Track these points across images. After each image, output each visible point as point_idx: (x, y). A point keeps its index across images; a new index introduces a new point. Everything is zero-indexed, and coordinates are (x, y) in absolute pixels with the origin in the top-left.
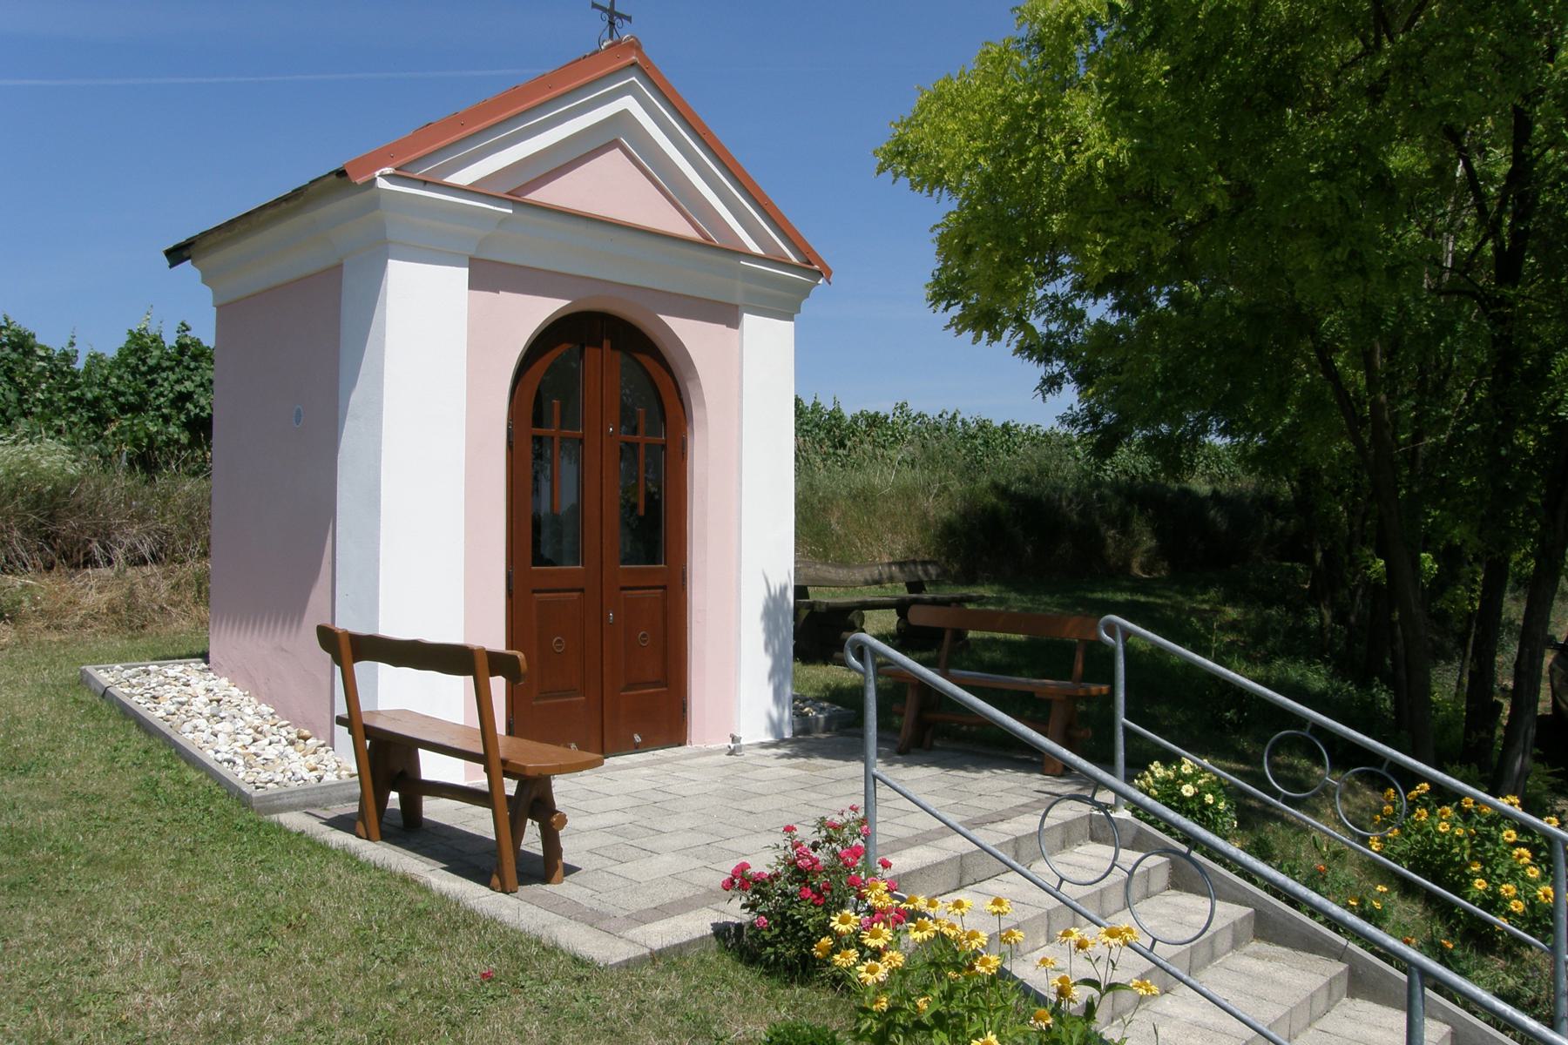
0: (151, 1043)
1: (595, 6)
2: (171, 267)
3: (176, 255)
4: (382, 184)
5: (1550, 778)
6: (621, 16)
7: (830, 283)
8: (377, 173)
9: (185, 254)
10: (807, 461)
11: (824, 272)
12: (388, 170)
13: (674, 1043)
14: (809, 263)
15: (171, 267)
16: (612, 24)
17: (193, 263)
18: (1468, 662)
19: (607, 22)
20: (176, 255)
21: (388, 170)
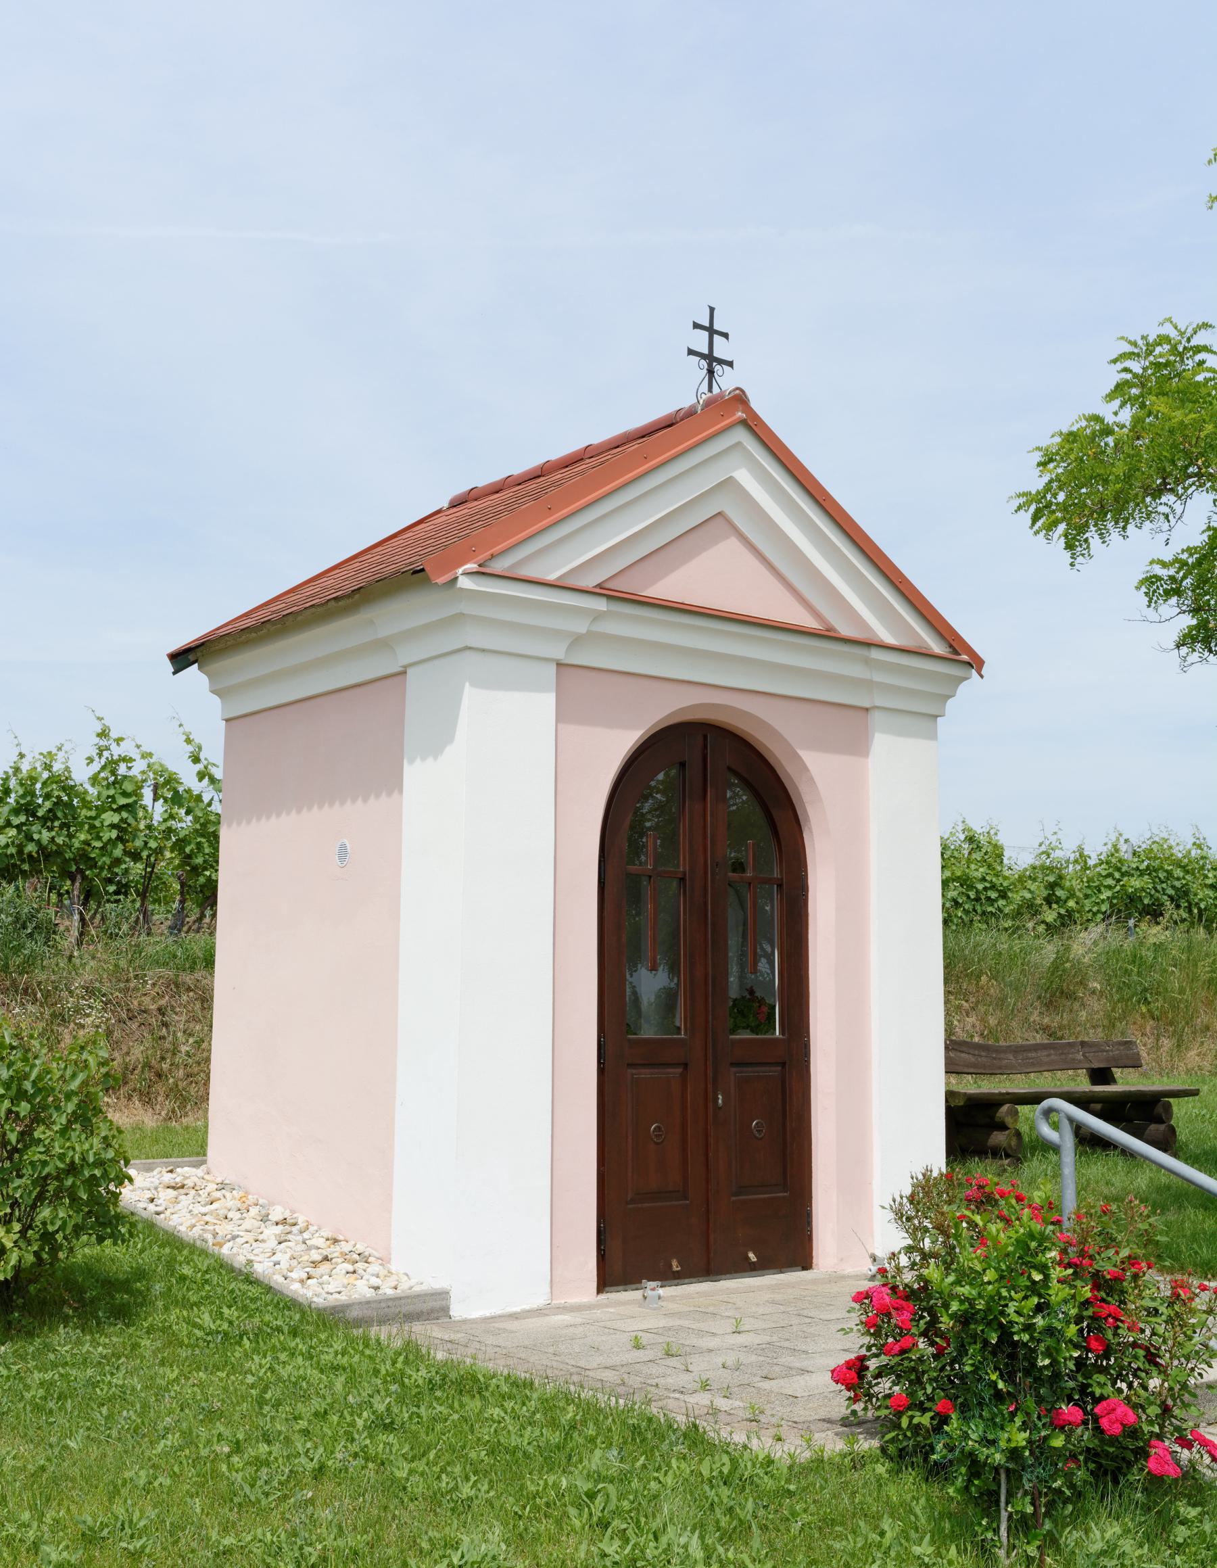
0: (469, 1566)
1: (691, 352)
2: (174, 673)
3: (181, 659)
4: (465, 583)
5: (1039, 524)
6: (721, 362)
7: (982, 677)
8: (460, 571)
9: (191, 657)
10: (638, 829)
11: (976, 663)
12: (471, 566)
13: (1132, 1565)
14: (956, 652)
15: (174, 673)
16: (711, 372)
17: (200, 668)
18: (405, 655)
19: (705, 371)
20: (181, 659)
21: (471, 566)
